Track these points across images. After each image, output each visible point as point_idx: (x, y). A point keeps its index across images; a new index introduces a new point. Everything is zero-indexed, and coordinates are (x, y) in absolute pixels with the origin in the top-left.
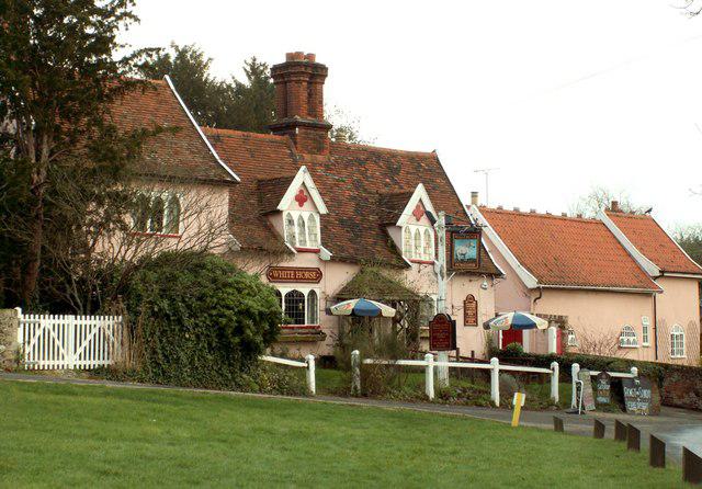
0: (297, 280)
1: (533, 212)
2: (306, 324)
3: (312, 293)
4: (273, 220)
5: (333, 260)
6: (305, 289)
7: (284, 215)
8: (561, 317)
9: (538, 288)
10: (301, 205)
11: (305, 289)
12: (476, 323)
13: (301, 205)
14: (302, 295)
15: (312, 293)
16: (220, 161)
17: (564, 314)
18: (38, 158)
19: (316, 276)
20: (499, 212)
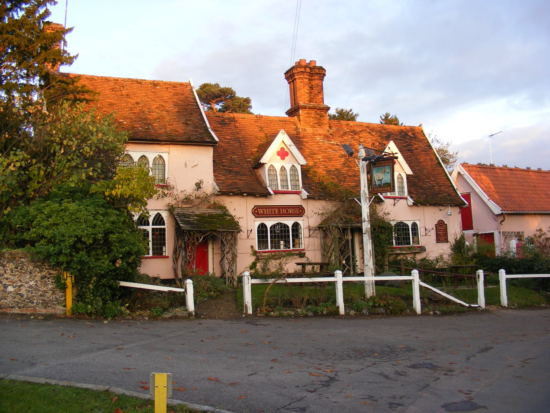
0: (280, 215)
1: (540, 169)
2: (270, 249)
3: (296, 226)
4: (260, 171)
5: (309, 198)
6: (289, 222)
7: (267, 167)
8: (518, 233)
9: (502, 214)
10: (283, 158)
11: (289, 222)
12: (446, 241)
13: (283, 158)
14: (286, 226)
15: (296, 226)
16: (210, 130)
17: (520, 231)
18: (21, 375)
19: (299, 211)
20: (481, 167)
